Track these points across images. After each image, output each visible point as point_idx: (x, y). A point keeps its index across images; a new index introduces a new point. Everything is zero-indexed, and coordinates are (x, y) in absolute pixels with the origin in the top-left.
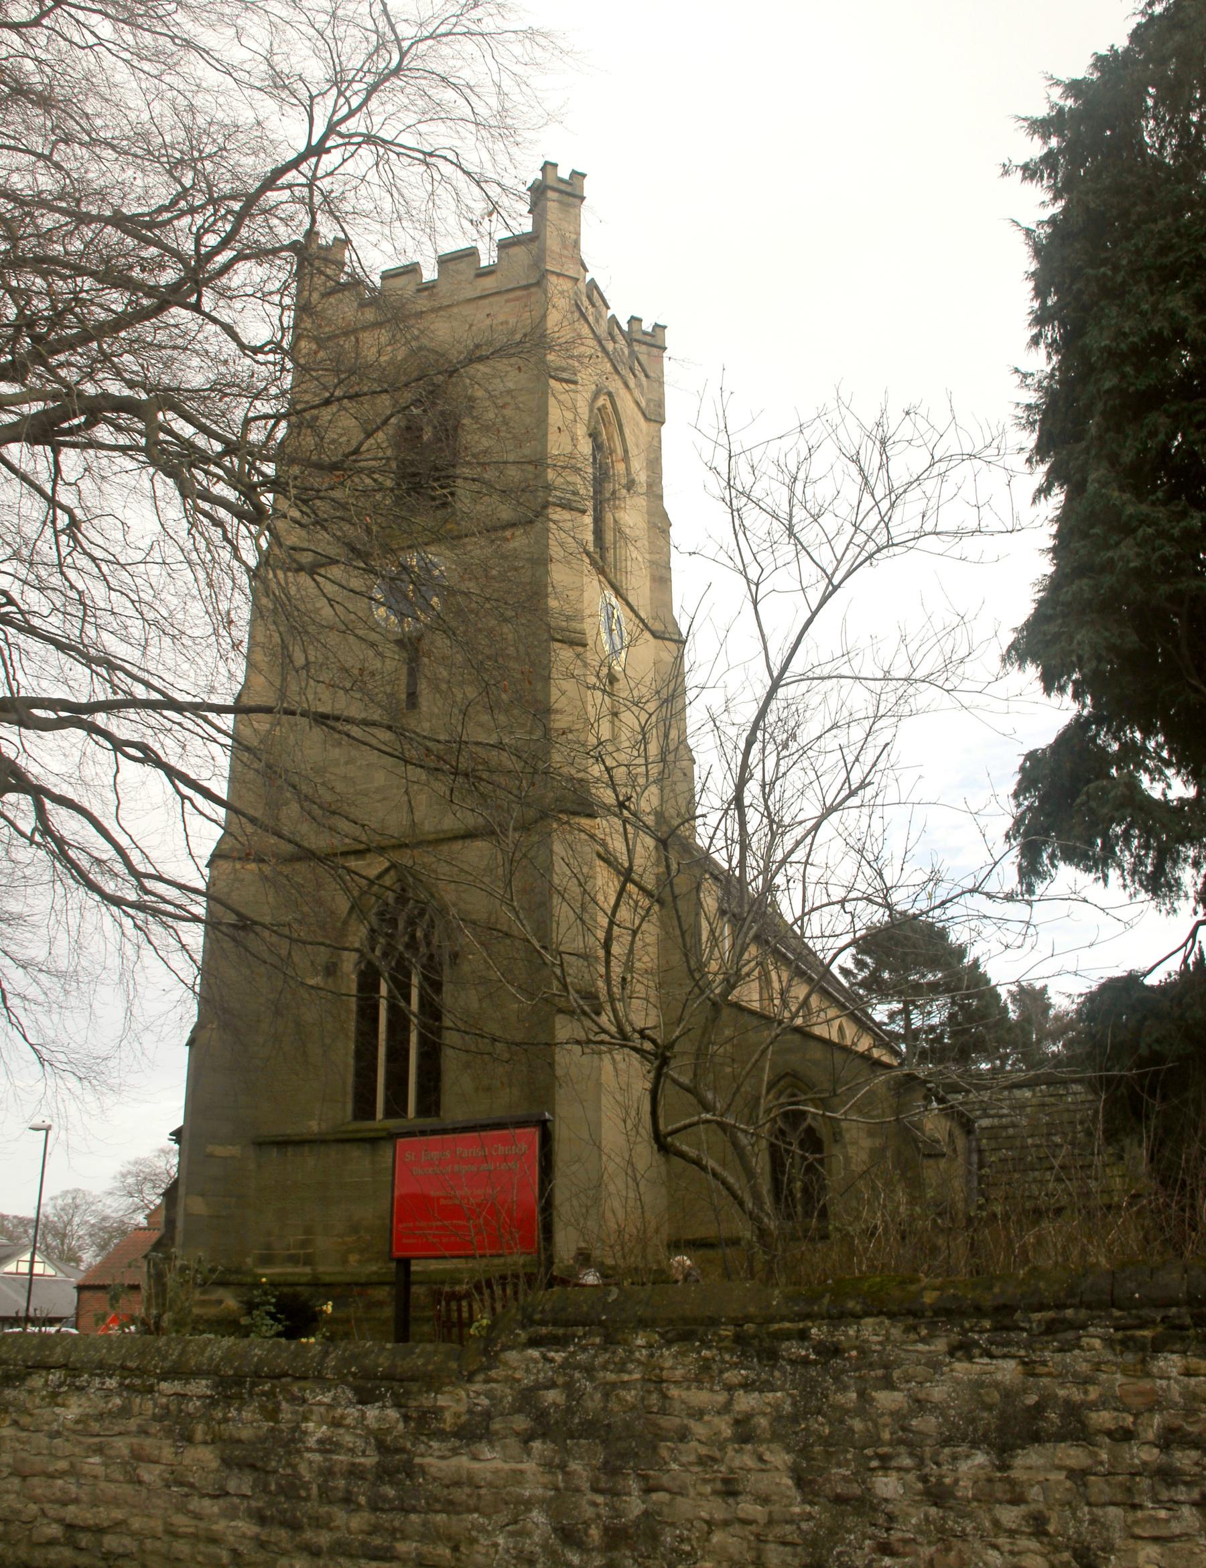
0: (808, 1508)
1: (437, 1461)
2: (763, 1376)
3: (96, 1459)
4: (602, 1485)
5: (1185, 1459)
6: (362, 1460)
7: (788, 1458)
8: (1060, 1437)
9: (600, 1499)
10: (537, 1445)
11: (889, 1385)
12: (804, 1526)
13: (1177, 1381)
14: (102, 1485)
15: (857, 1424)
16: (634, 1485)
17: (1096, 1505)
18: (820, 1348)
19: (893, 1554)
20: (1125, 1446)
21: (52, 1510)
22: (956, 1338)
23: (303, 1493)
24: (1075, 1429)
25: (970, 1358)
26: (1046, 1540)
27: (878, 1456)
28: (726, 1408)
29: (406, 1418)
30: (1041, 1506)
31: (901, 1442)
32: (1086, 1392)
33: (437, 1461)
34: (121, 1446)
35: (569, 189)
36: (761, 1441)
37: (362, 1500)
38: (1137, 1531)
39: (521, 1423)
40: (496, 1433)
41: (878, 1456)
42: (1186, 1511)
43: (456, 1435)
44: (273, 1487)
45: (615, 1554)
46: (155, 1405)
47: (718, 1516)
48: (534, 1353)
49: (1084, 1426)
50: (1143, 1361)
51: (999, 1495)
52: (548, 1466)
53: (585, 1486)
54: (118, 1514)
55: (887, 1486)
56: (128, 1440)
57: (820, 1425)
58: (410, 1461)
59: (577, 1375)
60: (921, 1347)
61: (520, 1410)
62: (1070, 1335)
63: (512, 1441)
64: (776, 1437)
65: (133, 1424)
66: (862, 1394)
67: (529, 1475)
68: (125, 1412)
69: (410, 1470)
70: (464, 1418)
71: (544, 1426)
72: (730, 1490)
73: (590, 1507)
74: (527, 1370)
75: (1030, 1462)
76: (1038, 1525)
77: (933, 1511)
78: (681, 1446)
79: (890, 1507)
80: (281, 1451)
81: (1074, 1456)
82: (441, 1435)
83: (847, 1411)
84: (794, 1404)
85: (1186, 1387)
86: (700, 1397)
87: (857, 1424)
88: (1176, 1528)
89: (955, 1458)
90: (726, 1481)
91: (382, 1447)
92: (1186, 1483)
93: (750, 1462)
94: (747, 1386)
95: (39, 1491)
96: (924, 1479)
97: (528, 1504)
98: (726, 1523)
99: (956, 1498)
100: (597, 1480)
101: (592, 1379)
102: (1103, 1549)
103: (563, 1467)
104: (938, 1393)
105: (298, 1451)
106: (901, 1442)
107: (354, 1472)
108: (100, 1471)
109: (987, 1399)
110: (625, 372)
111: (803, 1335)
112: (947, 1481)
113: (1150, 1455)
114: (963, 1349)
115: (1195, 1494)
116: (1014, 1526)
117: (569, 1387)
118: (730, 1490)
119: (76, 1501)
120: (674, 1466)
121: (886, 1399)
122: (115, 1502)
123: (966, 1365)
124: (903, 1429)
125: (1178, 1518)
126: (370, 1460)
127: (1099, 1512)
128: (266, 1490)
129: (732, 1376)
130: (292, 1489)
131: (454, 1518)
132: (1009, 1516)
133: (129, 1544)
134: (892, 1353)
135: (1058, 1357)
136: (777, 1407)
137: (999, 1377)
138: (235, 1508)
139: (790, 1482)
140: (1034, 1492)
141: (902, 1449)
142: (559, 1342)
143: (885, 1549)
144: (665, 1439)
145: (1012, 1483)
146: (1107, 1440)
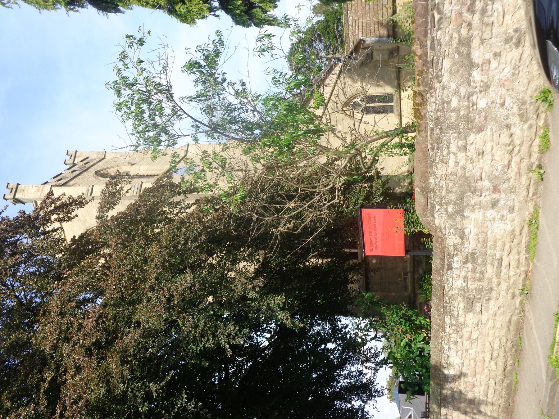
0: (489, 129)
1: (470, 247)
2: (445, 143)
3: (470, 351)
4: (479, 194)
5: (479, 5)
6: (470, 268)
7: (472, 135)
8: (470, 47)
9: (484, 194)
10: (466, 214)
11: (449, 103)
12: (494, 131)
13: (453, 7)
14: (478, 349)
15: (462, 113)
16: (480, 184)
17: (492, 36)
18: (436, 124)
19: (504, 102)
20: (473, 26)
21: (486, 365)
22: (435, 81)
23: (481, 287)
24: (466, 42)
25: (442, 76)
26: (502, 53)
27: (473, 106)
28: (455, 154)
29: (457, 254)
30: (492, 54)
31: (468, 98)
32: (455, 38)
33: (470, 247)
34: (467, 344)
35: (14, 190)
36: (467, 144)
37: (483, 269)
38: (501, 22)
39: (459, 219)
40: (462, 226)
41: (473, 106)
42: (495, 6)
43: (462, 240)
44: (479, 296)
45: (501, 190)
46: (453, 333)
47: (490, 157)
48: (436, 215)
49: (466, 38)
50: (446, 18)
51: (487, 68)
52: (473, 210)
53: (480, 199)
54: (488, 344)
55: (482, 103)
56: (464, 342)
57: (461, 125)
58: (471, 254)
59: (444, 201)
60: (437, 92)
61: (455, 219)
62: (436, 42)
63: (464, 222)
64: (466, 138)
65: (459, 340)
66: (452, 111)
67: (476, 217)
68: (456, 343)
69: (473, 254)
70: (457, 237)
71: (460, 212)
72: (481, 154)
73: (487, 198)
74: (442, 217)
75: (477, 56)
76: (497, 55)
77: (491, 89)
78: (467, 169)
79: (489, 103)
80: (467, 294)
81: (476, 42)
82: (462, 244)
83: (458, 116)
84: (455, 133)
85: (455, 4)
86: (451, 163)
87: (462, 113)
88: (500, 10)
89: (474, 82)
90: (479, 155)
91: (466, 262)
92: (486, 6)
93: (473, 146)
94: (448, 147)
95: (480, 369)
96: (481, 92)
97: (485, 216)
98: (493, 155)
99: (487, 82)
100: (478, 195)
101: (445, 197)
102: (506, 34)
103: (473, 206)
104: (453, 86)
105: (467, 288)
106: (468, 98)
107: (474, 271)
108: (474, 350)
109: (456, 70)
110: (88, 165)
111: (432, 129)
112: (482, 84)
113: (477, 17)
114: (438, 77)
115: (490, 3)
116: (497, 63)
117: (446, 204)
118: (481, 154)
119: (483, 357)
120: (473, 171)
121: (454, 103)
122: (484, 345)
123: (444, 77)
124: (464, 98)
125: (497, 10)
126: (470, 265)
127: (494, 35)
128: (480, 299)
129: (445, 153)
130: (479, 290)
131: (489, 240)
132: (494, 64)
133: (497, 340)
134: (439, 101)
135: (443, 47)
136: (456, 138)
137: (449, 66)
138: (485, 308)
139: (480, 135)
140: (487, 56)
141: (471, 99)
142: (433, 207)
143: (503, 105)
144: (465, 174)
145: (483, 64)
146: (471, 31)
